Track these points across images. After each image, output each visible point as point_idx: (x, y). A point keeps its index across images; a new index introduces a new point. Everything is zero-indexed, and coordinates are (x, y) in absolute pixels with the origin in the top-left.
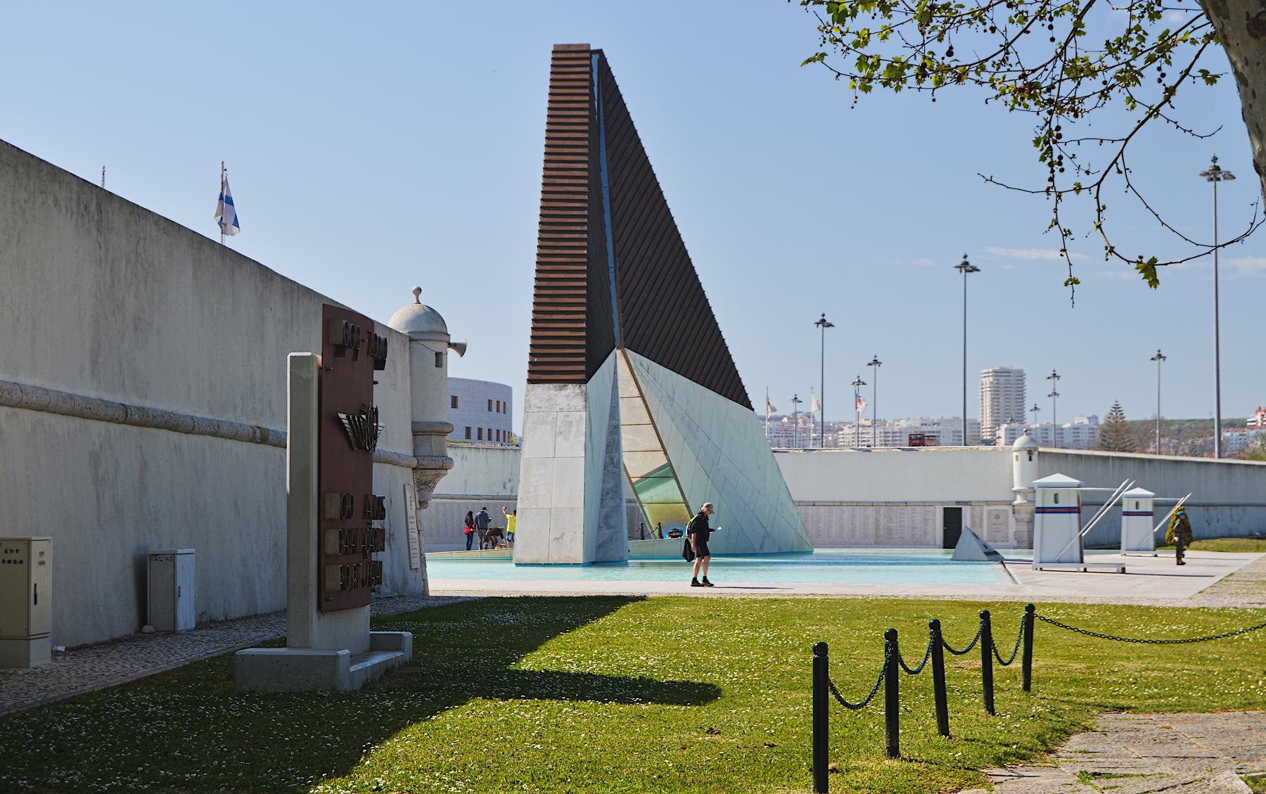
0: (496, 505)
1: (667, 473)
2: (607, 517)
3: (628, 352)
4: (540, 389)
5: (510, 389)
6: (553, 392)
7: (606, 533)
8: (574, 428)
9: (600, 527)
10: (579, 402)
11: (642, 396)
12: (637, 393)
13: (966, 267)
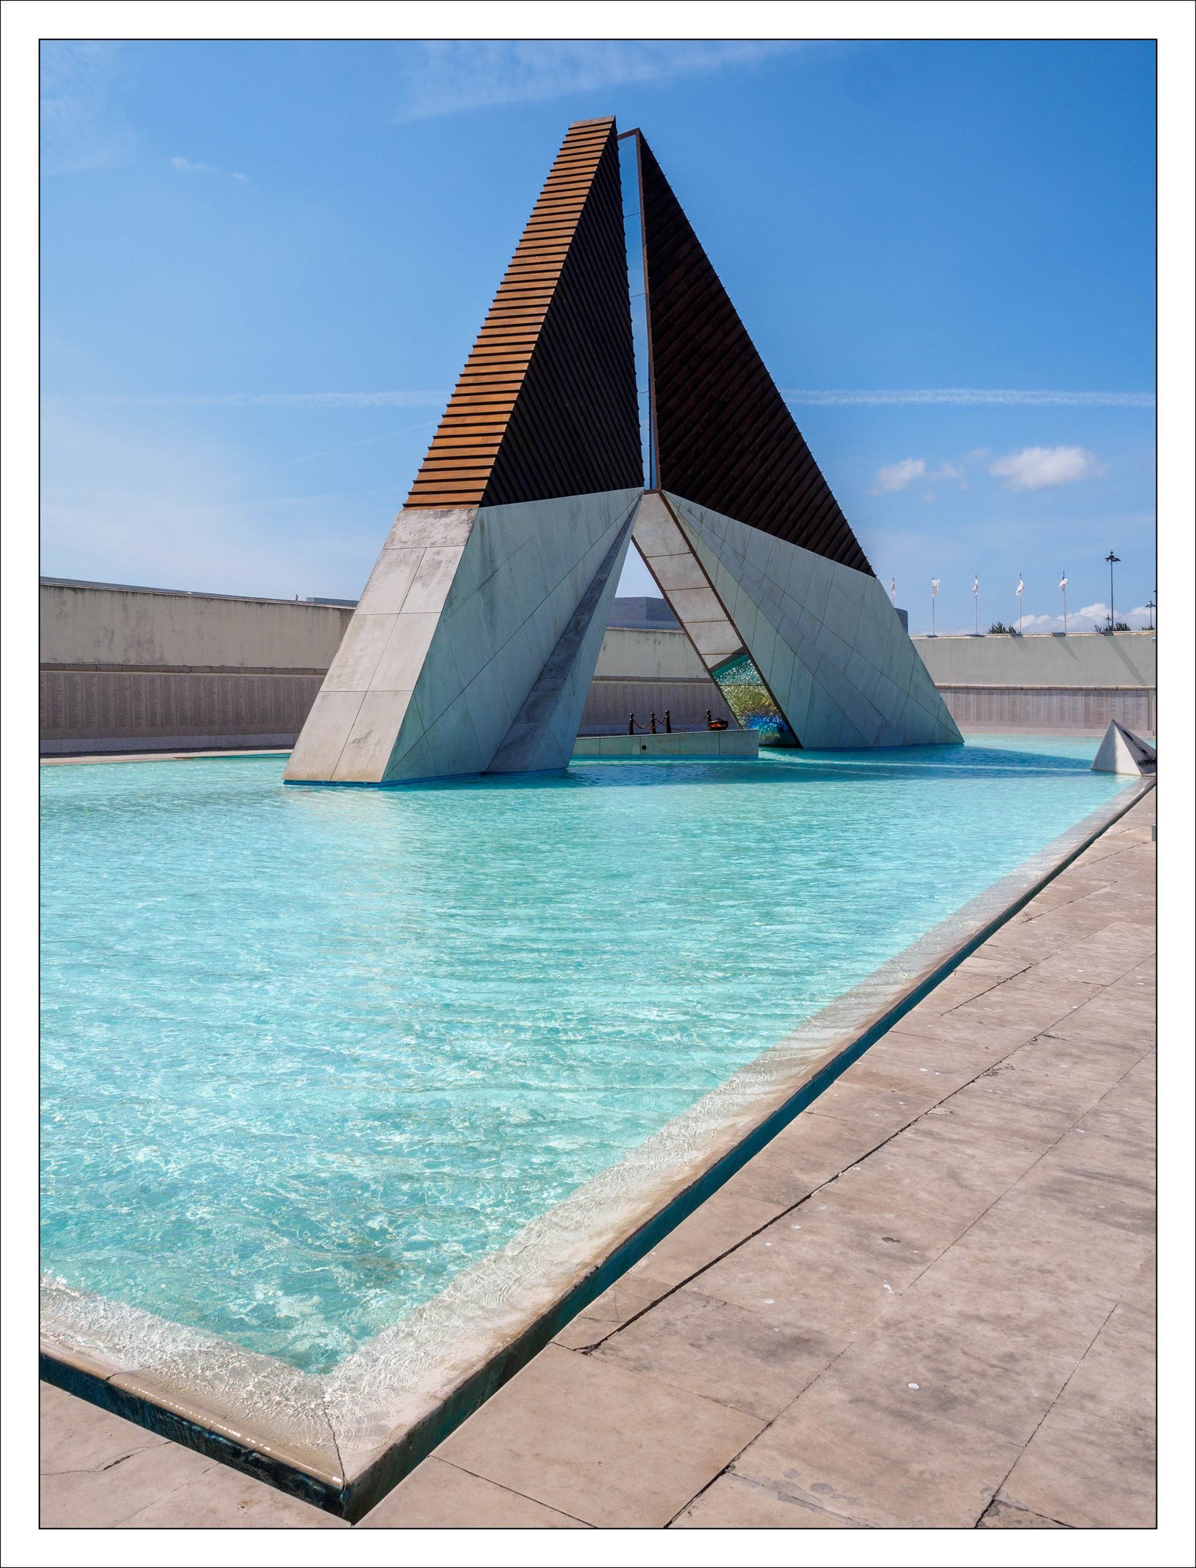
0: (626, 686)
1: (742, 656)
2: (535, 704)
3: (667, 494)
4: (415, 516)
5: (906, 612)
6: (431, 520)
7: (523, 727)
8: (441, 571)
9: (516, 720)
10: (461, 533)
11: (693, 551)
12: (687, 549)
13: (1112, 558)
